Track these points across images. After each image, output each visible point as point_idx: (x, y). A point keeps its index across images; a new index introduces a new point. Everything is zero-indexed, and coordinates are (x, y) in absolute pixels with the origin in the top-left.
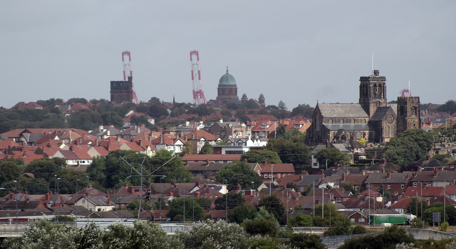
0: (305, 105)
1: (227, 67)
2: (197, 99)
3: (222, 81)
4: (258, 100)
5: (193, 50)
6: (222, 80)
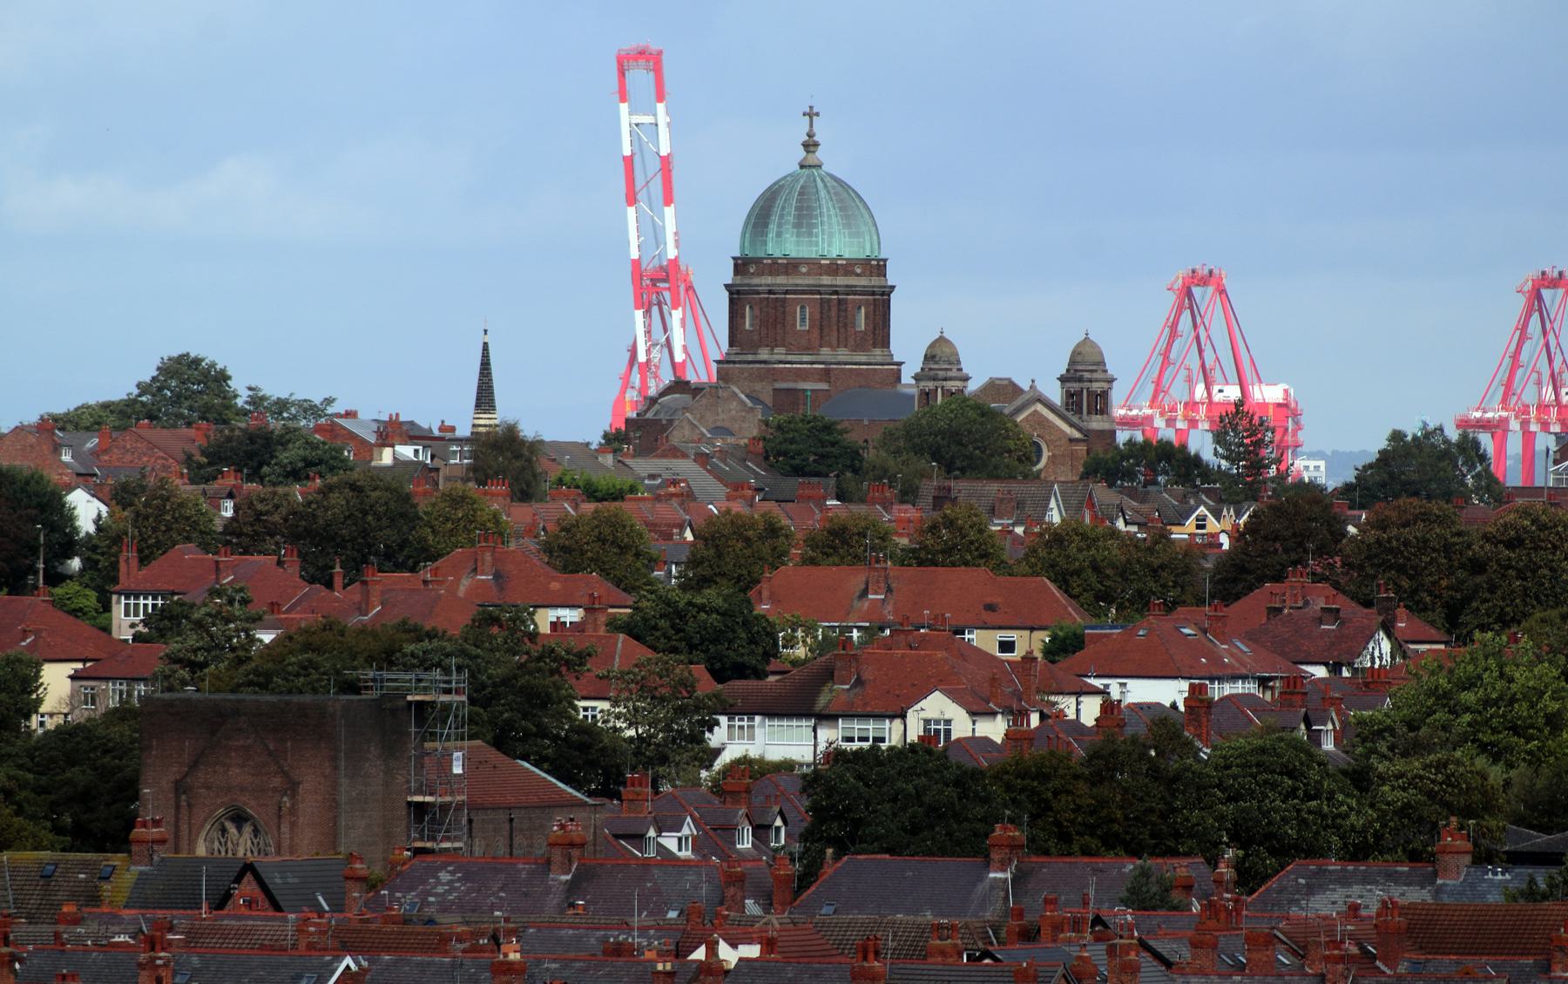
0: (1446, 441)
1: (811, 114)
2: (655, 309)
3: (766, 225)
4: (1055, 394)
5: (630, 43)
6: (761, 217)
